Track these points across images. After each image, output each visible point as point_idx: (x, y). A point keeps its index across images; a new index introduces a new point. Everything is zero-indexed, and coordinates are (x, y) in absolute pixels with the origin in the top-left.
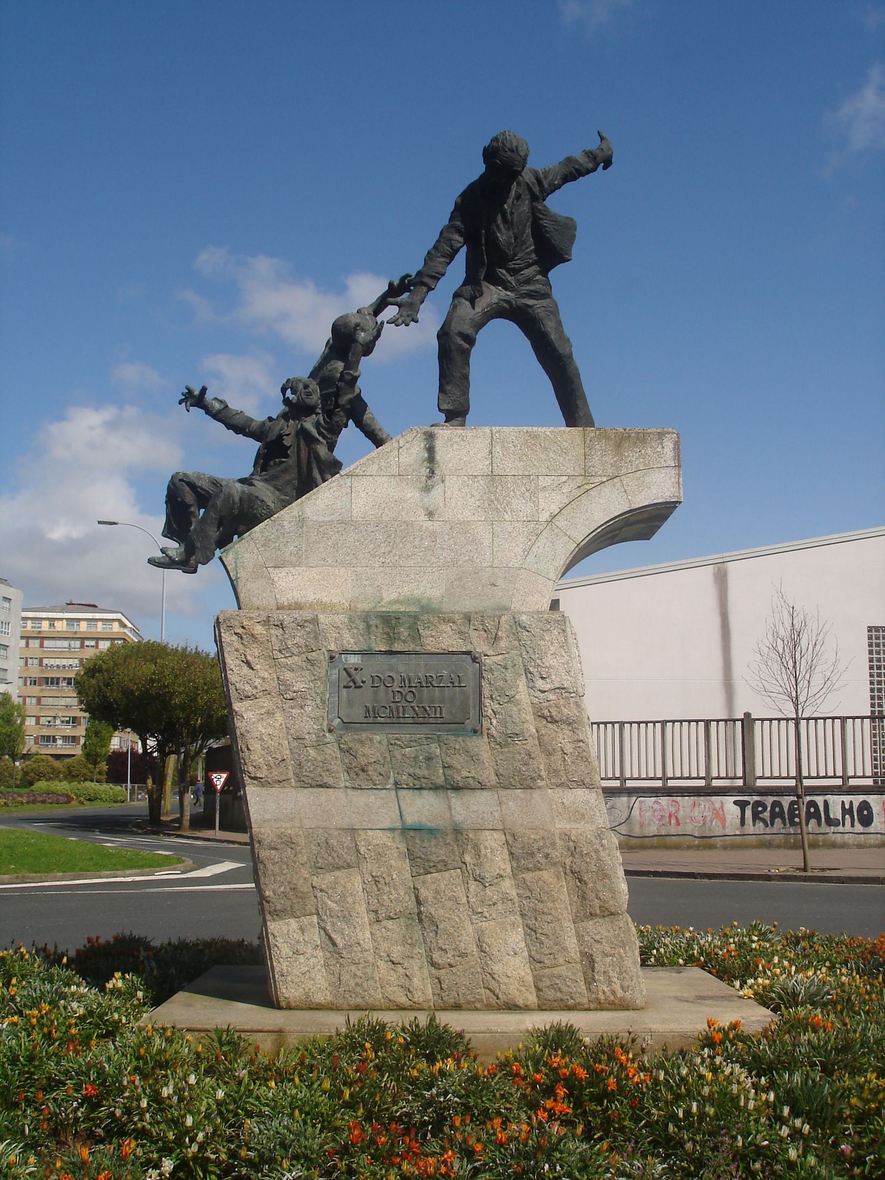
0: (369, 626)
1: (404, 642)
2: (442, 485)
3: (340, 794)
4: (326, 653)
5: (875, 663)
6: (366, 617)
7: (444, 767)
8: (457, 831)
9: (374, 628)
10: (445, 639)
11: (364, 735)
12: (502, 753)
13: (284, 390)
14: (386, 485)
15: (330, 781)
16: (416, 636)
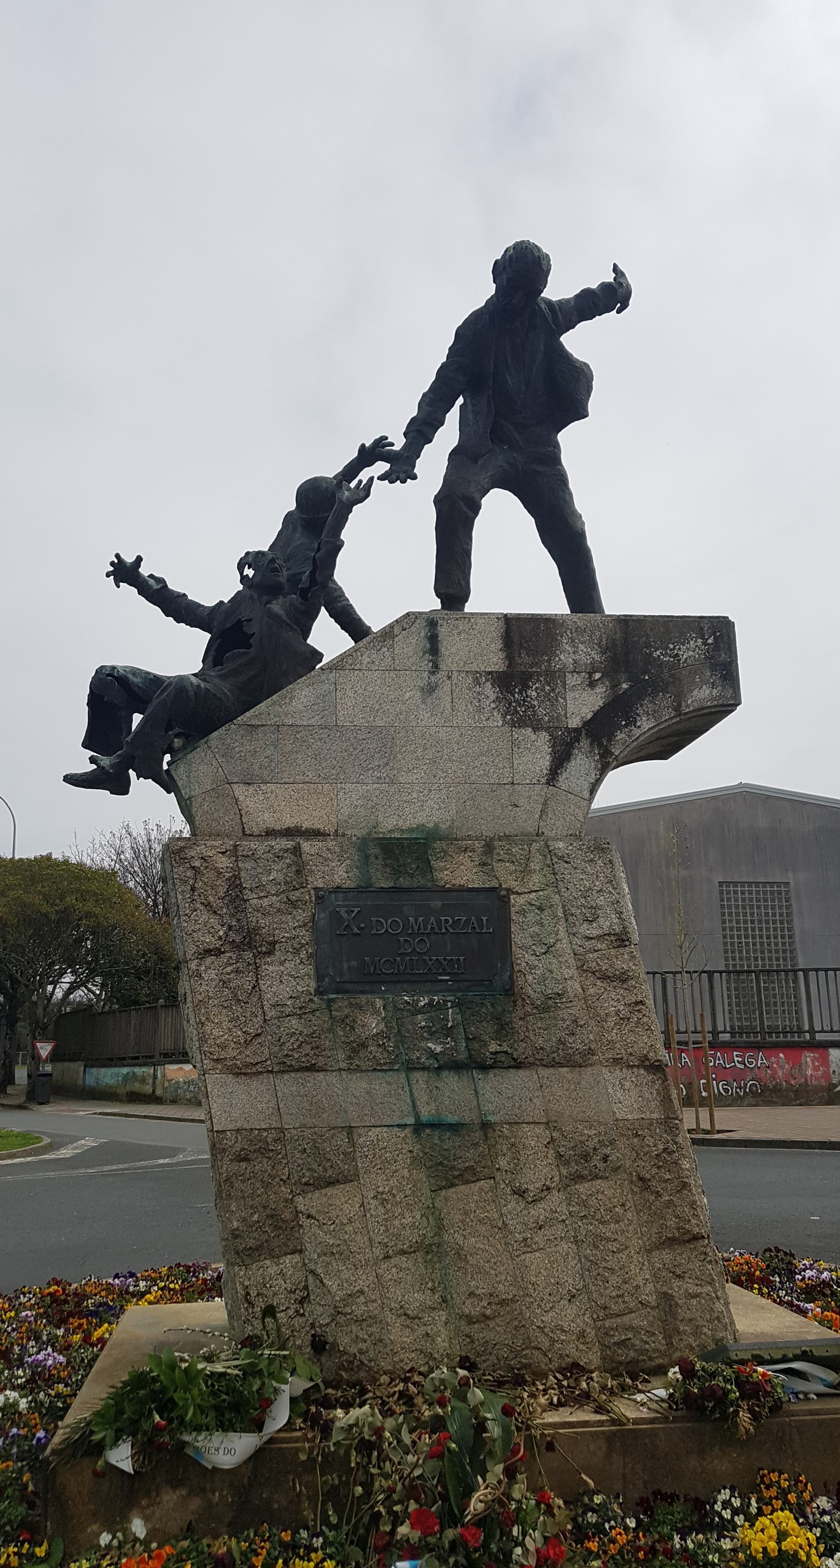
0: (367, 857)
1: (412, 876)
2: (448, 682)
3: (333, 1078)
4: (312, 892)
5: (762, 903)
6: (363, 844)
7: (467, 1039)
8: (486, 1126)
9: (373, 859)
10: (460, 872)
11: (363, 998)
12: (541, 1018)
13: (241, 567)
14: (379, 681)
15: (321, 1061)
16: (427, 868)
